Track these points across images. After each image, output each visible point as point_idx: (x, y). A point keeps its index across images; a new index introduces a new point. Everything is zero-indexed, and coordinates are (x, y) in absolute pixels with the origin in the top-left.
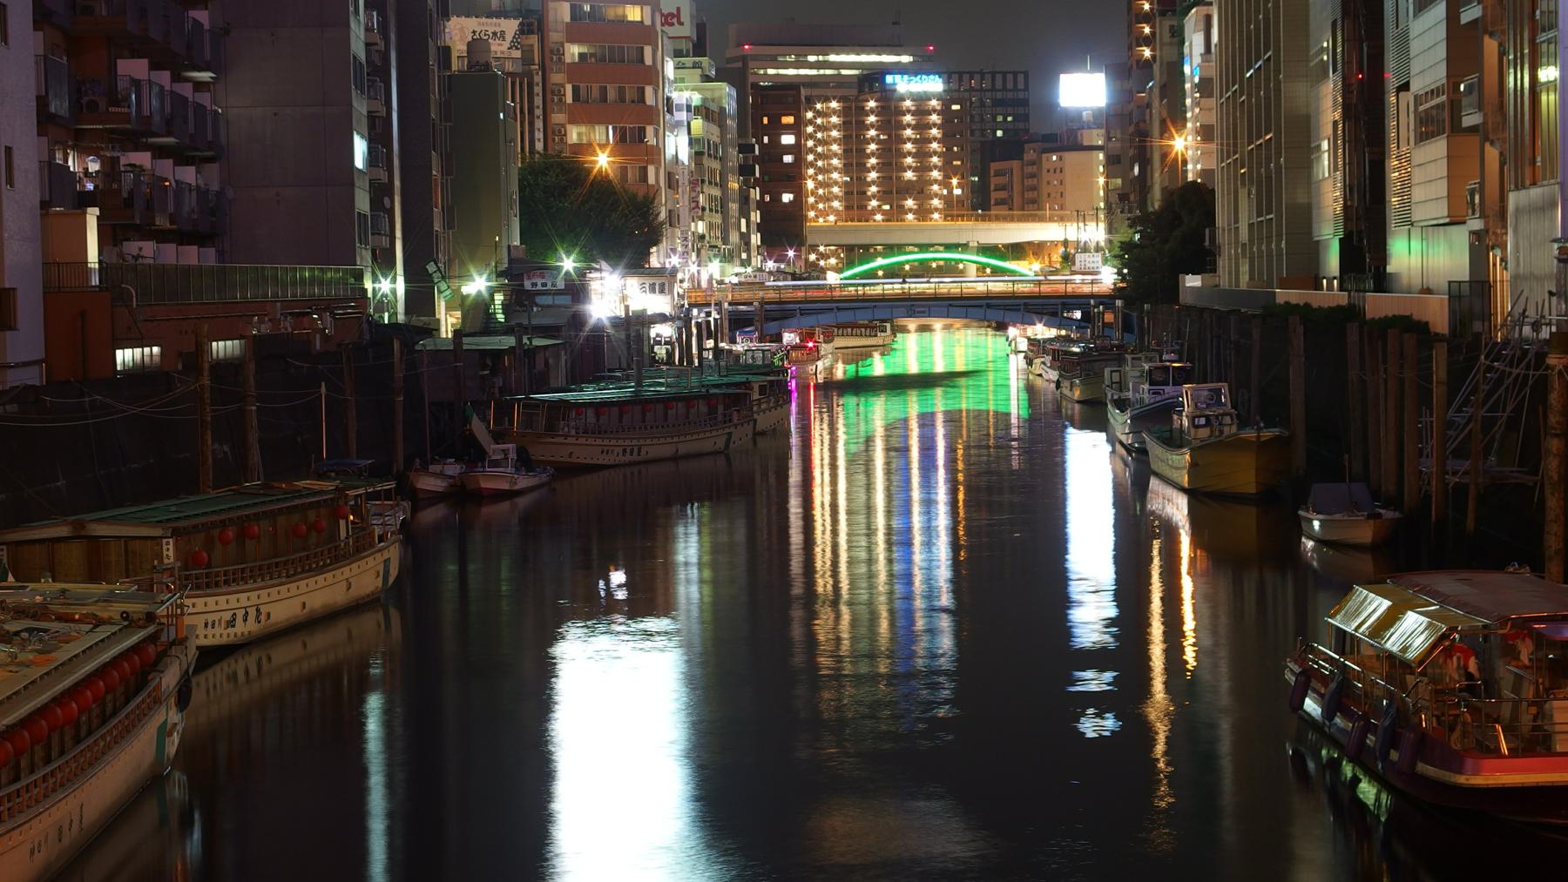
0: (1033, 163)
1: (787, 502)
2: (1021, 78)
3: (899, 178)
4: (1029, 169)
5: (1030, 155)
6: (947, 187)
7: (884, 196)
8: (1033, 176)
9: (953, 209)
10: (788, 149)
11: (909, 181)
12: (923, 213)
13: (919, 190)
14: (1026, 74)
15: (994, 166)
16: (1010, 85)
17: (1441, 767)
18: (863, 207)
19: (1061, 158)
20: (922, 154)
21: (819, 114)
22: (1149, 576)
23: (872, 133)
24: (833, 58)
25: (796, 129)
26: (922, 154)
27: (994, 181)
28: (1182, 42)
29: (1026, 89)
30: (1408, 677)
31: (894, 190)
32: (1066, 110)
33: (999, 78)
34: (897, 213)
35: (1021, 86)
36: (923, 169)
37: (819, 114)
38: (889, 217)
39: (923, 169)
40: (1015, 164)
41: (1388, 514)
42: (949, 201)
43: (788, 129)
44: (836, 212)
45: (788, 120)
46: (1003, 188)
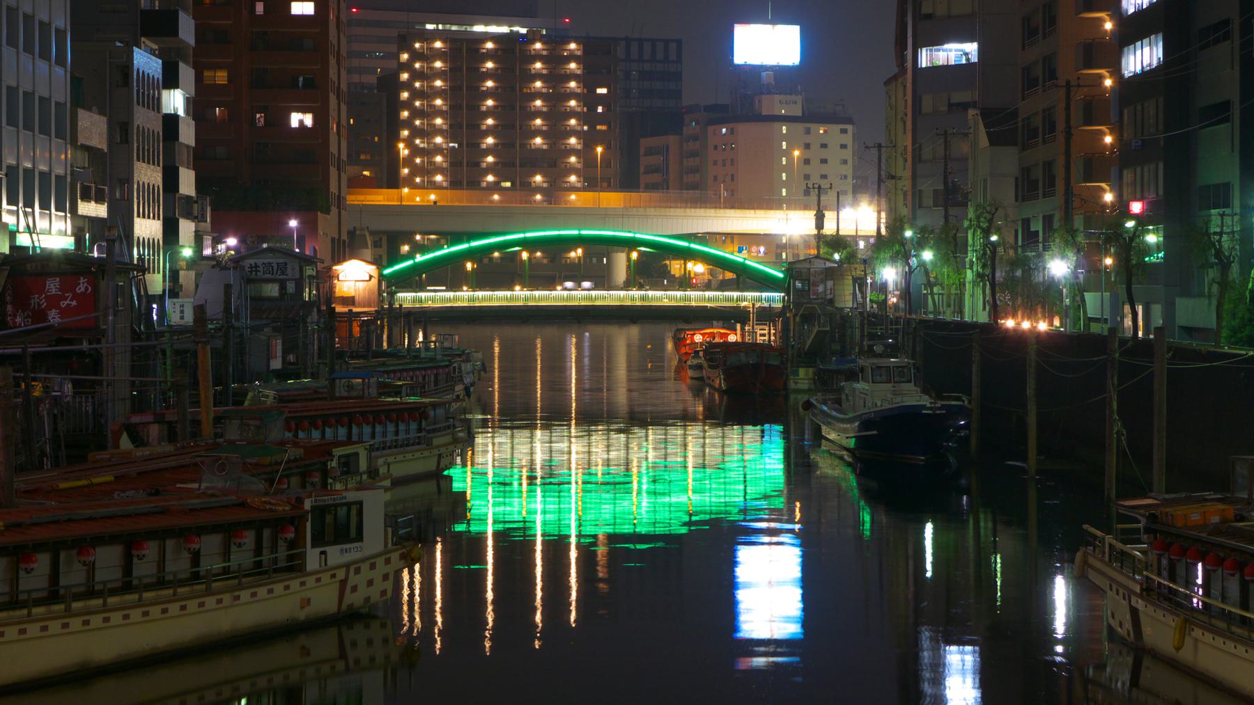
0: (696, 138)
1: (947, 69)
2: (673, 46)
3: (523, 146)
8: (693, 154)
11: (539, 150)
12: (555, 189)
13: (552, 162)
14: (679, 42)
15: (645, 143)
16: (660, 56)
19: (731, 131)
20: (556, 116)
21: (416, 56)
22: (934, 555)
24: (406, 598)
26: (556, 116)
27: (645, 161)
29: (679, 60)
30: (317, 474)
31: (517, 162)
32: (739, 66)
33: (647, 47)
35: (673, 57)
36: (556, 133)
37: (416, 56)
39: (556, 133)
40: (672, 140)
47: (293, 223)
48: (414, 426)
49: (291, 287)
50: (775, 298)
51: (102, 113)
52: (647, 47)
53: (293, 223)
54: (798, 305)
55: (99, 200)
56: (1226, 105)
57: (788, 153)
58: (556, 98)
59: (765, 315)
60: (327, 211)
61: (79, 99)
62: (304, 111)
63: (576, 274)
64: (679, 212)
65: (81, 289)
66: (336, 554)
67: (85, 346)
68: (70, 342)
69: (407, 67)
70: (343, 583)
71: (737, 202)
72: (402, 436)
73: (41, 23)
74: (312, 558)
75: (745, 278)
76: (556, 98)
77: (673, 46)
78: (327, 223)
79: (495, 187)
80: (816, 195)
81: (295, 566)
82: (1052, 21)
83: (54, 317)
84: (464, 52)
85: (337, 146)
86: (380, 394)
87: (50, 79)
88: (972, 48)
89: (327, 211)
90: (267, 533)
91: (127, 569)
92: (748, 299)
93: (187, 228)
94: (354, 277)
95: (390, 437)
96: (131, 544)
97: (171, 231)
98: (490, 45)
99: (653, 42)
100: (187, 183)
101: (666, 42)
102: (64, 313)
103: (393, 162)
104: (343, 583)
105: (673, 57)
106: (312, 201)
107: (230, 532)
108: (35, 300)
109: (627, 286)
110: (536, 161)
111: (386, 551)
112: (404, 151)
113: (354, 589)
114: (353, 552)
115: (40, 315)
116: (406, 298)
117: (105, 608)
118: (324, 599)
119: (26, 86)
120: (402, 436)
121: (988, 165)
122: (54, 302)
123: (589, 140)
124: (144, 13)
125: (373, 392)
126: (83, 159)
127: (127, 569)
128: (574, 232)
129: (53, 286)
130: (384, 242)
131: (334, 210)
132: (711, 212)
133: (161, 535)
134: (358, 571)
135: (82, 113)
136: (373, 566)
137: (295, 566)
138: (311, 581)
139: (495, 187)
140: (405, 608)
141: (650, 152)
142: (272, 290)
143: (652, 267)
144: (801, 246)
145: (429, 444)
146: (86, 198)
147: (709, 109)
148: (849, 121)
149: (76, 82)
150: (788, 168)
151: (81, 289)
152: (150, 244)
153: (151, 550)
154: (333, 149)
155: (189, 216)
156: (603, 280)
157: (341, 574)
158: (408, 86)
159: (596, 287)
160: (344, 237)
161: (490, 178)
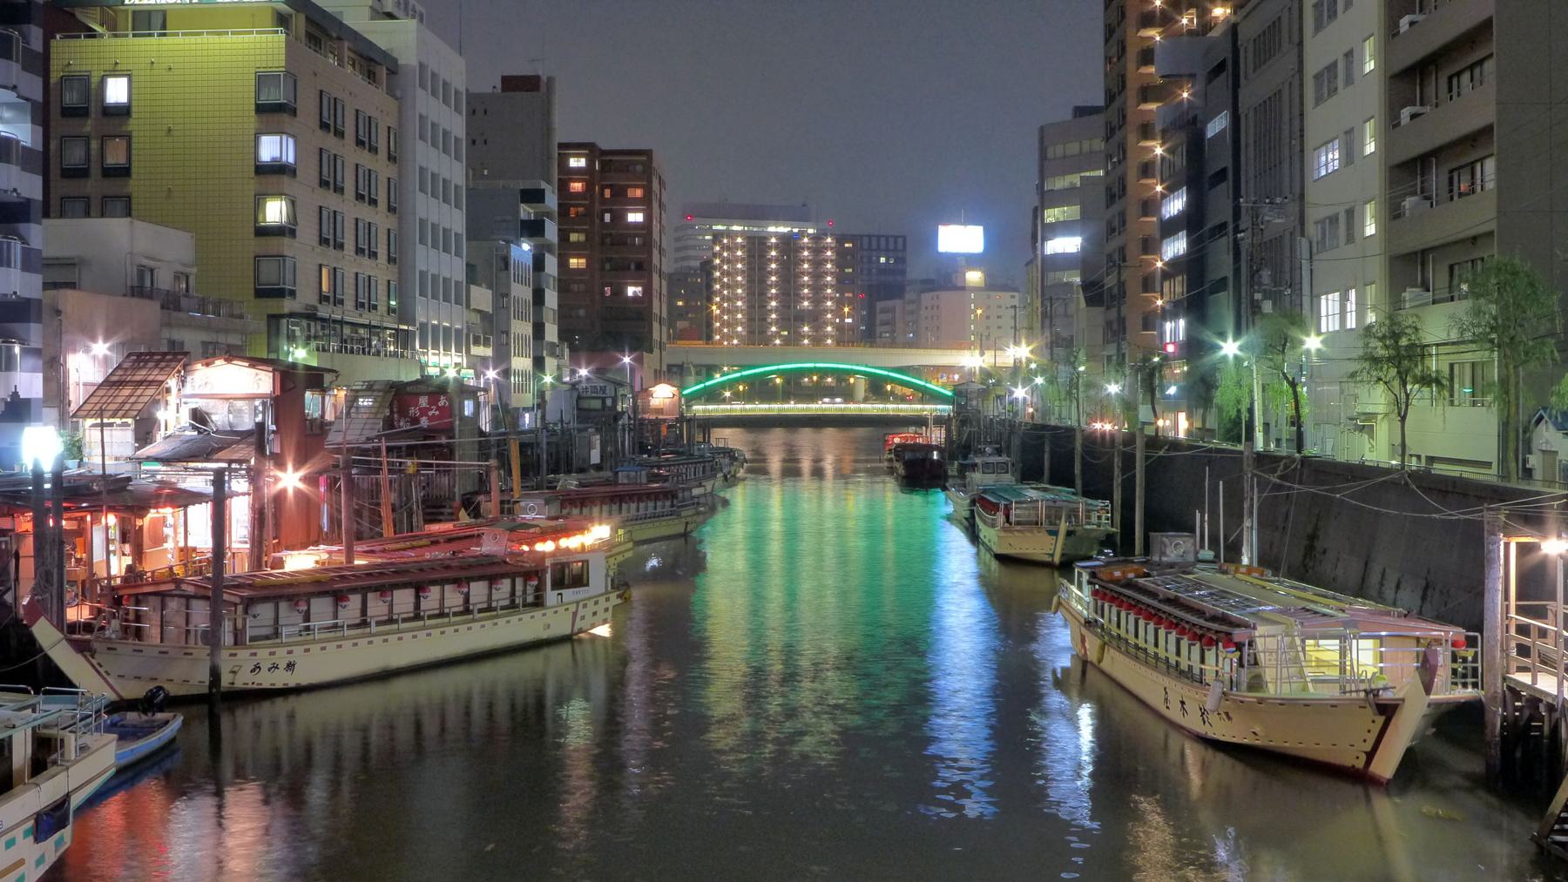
0: (912, 302)
2: (900, 241)
4: (909, 307)
5: (909, 296)
6: (840, 314)
7: (784, 322)
8: (912, 312)
9: (845, 338)
10: (577, 250)
13: (815, 318)
14: (904, 238)
15: (880, 305)
17: (1073, 459)
18: (763, 331)
20: (817, 288)
23: (773, 253)
25: (645, 203)
26: (817, 288)
27: (880, 317)
28: (1499, 206)
31: (791, 319)
33: (883, 241)
34: (793, 340)
35: (900, 247)
36: (818, 299)
38: (787, 342)
39: (818, 299)
40: (897, 303)
41: (1489, 398)
42: (840, 328)
43: (635, 204)
44: (738, 336)
45: (577, 186)
46: (886, 323)
47: (627, 360)
48: (668, 503)
49: (609, 402)
50: (945, 409)
51: (490, 287)
52: (883, 241)
53: (627, 360)
54: (958, 414)
55: (486, 344)
56: (1224, 279)
57: (974, 312)
58: (817, 275)
59: (939, 421)
60: (651, 351)
61: (472, 275)
62: (636, 285)
63: (831, 393)
64: (859, 350)
65: (441, 403)
66: (569, 594)
67: (444, 441)
68: (434, 438)
69: (719, 255)
70: (575, 614)
71: (938, 345)
72: (659, 510)
73: (445, 230)
74: (551, 596)
75: (928, 396)
76: (817, 275)
77: (900, 241)
78: (651, 360)
79: (777, 335)
80: (987, 342)
81: (539, 603)
82: (1124, 223)
83: (424, 423)
84: (756, 246)
85: (659, 308)
86: (650, 482)
87: (453, 268)
88: (583, 261)
89: (651, 351)
90: (519, 581)
91: (417, 606)
92: (928, 409)
93: (550, 363)
94: (662, 394)
95: (651, 510)
96: (420, 589)
97: (539, 363)
98: (773, 240)
99: (887, 238)
100: (551, 333)
101: (896, 238)
102: (431, 419)
103: (709, 319)
104: (575, 614)
105: (900, 247)
106: (641, 344)
107: (492, 580)
108: (412, 411)
109: (865, 400)
110: (801, 318)
111: (607, 592)
112: (715, 310)
113: (583, 618)
114: (581, 593)
115: (415, 420)
116: (699, 409)
117: (399, 631)
118: (561, 627)
119: (433, 270)
120: (659, 510)
121: (1084, 318)
122: (424, 412)
123: (840, 303)
124: (523, 222)
125: (644, 480)
126: (476, 318)
127: (417, 606)
128: (811, 365)
129: (423, 401)
130: (675, 373)
131: (656, 351)
132: (921, 351)
133: (442, 582)
134: (585, 606)
135: (473, 287)
136: (596, 603)
137: (539, 603)
138: (549, 612)
139: (777, 335)
140: (1500, 596)
141: (883, 311)
142: (597, 404)
143: (876, 388)
144: (977, 378)
145: (679, 515)
146: (477, 342)
147: (924, 282)
148: (1015, 290)
149: (471, 268)
150: (975, 322)
151: (441, 403)
152: (524, 374)
153: (434, 591)
154: (656, 310)
155: (553, 354)
156: (848, 396)
157: (573, 608)
158: (720, 267)
159: (846, 401)
160: (665, 368)
161: (774, 329)
